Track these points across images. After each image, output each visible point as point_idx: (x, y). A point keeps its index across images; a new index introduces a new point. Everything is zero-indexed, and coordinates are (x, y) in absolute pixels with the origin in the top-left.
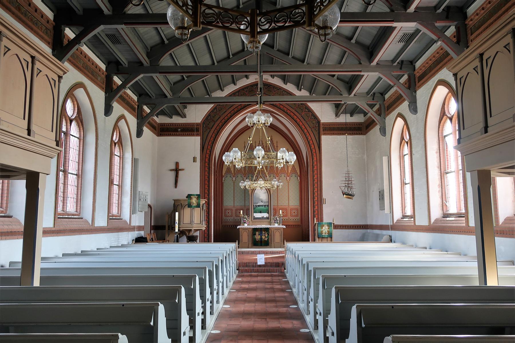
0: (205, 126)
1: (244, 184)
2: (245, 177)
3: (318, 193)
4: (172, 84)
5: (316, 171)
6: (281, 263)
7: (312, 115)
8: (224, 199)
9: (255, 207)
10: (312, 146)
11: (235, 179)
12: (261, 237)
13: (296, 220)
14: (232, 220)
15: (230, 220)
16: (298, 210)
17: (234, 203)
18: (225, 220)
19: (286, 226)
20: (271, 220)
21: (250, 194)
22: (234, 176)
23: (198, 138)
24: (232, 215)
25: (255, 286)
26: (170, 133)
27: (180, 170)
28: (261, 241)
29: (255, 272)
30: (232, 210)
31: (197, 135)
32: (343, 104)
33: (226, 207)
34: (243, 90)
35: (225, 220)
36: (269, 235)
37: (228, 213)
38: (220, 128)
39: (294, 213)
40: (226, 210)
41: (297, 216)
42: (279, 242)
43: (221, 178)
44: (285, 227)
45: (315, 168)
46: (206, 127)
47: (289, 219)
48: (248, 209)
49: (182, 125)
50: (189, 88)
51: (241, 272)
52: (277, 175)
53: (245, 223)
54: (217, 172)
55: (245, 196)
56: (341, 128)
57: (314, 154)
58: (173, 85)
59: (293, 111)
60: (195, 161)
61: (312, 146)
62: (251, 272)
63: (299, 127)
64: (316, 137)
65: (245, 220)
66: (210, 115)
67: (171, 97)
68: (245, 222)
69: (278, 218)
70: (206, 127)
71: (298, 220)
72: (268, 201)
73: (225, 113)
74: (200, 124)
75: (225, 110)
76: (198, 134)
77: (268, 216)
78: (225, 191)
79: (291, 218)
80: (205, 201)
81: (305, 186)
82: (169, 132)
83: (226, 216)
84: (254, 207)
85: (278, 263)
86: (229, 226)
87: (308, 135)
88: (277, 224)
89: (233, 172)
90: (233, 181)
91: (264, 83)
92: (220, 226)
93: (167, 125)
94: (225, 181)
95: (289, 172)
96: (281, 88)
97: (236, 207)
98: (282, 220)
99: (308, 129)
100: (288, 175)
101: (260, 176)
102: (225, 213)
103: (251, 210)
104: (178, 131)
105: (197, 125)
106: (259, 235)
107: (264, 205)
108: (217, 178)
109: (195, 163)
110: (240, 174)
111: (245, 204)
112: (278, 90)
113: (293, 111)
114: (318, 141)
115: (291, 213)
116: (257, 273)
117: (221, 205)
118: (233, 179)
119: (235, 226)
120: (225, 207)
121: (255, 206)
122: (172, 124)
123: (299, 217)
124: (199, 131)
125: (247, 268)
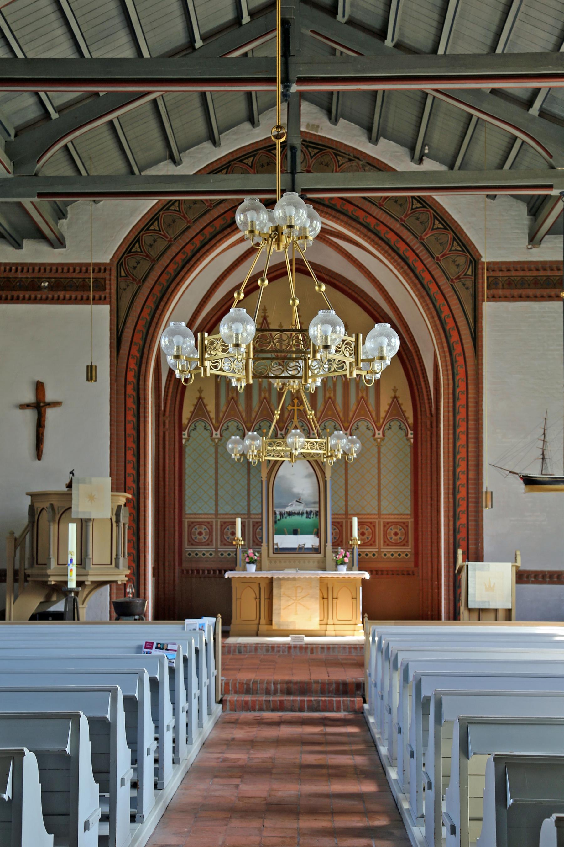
0: (123, 274)
1: (240, 447)
3: (470, 477)
4: (12, 133)
5: (463, 411)
6: (353, 683)
7: (454, 239)
8: (188, 492)
9: (278, 517)
10: (454, 334)
15: (197, 554)
18: (222, 555)
19: (371, 572)
20: (325, 556)
22: (216, 425)
23: (105, 309)
25: (270, 758)
26: (15, 294)
27: (49, 405)
29: (273, 710)
31: (99, 301)
32: (558, 199)
33: (192, 516)
34: (241, 161)
35: (190, 554)
38: (170, 280)
39: (396, 534)
40: (192, 525)
43: (177, 433)
45: (461, 402)
46: (126, 276)
48: (257, 523)
49: (54, 268)
50: (66, 146)
51: (231, 710)
54: (164, 415)
55: (249, 484)
56: (545, 278)
57: (460, 359)
58: (16, 135)
59: (397, 226)
60: (91, 379)
61: (454, 334)
62: (261, 710)
63: (414, 278)
64: (466, 307)
66: (138, 240)
67: (11, 176)
70: (126, 276)
71: (407, 555)
72: (318, 500)
73: (186, 233)
74: (108, 268)
75: (184, 226)
76: (103, 296)
77: (318, 544)
79: (385, 549)
80: (127, 499)
82: (14, 289)
83: (192, 543)
84: (276, 517)
85: (345, 684)
87: (441, 302)
89: (213, 415)
90: (213, 440)
91: (308, 139)
92: (177, 571)
93: (5, 268)
94: (190, 441)
95: (383, 414)
96: (358, 156)
97: (222, 516)
99: (442, 281)
100: (379, 425)
102: (190, 533)
103: (267, 525)
104: (40, 288)
105: (100, 271)
107: (307, 512)
108: (164, 433)
109: (92, 383)
110: (235, 421)
112: (350, 160)
113: (397, 226)
114: (471, 320)
115: (385, 534)
116: (280, 714)
117: (177, 510)
118: (214, 436)
119: (220, 571)
121: (278, 513)
122: (22, 267)
123: (409, 549)
124: (104, 289)
125: (249, 698)
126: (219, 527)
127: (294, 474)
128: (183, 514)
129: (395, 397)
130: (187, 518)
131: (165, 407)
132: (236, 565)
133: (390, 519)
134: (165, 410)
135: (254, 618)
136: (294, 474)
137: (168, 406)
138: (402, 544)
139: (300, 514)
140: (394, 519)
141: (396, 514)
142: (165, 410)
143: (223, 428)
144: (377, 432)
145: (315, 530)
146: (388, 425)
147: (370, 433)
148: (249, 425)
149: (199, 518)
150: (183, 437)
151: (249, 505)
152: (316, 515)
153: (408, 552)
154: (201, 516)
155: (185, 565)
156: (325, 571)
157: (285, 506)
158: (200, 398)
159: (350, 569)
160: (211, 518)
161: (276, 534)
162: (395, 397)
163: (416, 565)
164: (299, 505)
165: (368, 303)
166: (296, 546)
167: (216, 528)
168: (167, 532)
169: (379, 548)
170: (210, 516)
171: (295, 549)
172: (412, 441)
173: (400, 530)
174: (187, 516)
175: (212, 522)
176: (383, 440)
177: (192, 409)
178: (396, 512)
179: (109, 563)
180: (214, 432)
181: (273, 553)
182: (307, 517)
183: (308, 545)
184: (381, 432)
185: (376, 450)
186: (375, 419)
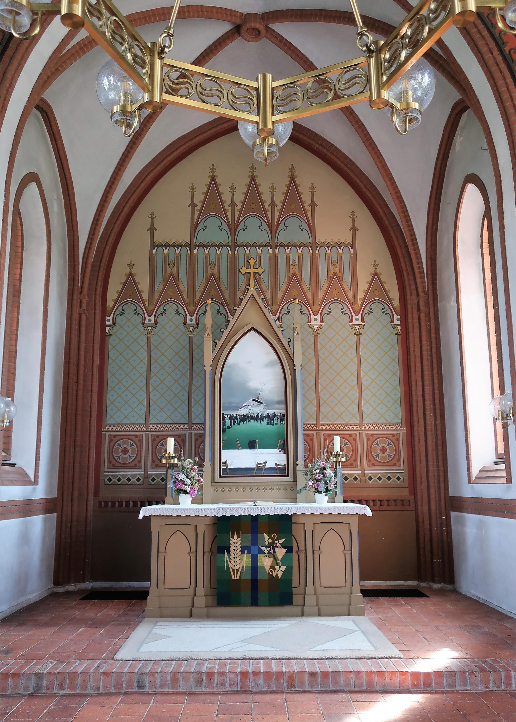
8: (111, 396)
9: (228, 423)
11: (153, 322)
12: (255, 560)
13: (389, 478)
14: (138, 480)
15: (119, 480)
16: (397, 439)
17: (148, 413)
18: (110, 480)
20: (295, 480)
21: (208, 369)
22: (150, 308)
24: (140, 462)
28: (255, 582)
33: (115, 428)
35: (153, 480)
36: (295, 549)
37: (125, 451)
39: (383, 450)
41: (394, 465)
42: (343, 583)
44: (368, 512)
47: (363, 475)
52: (315, 308)
53: (181, 491)
55: (191, 384)
65: (182, 477)
68: (183, 487)
69: (329, 472)
72: (284, 398)
77: (284, 463)
78: (112, 367)
79: (370, 471)
81: (424, 348)
83: (114, 464)
84: (224, 424)
86: (128, 503)
88: (326, 498)
89: (146, 296)
90: (145, 327)
92: (91, 503)
94: (117, 327)
95: (361, 295)
97: (154, 427)
98: (346, 479)
100: (356, 308)
102: (111, 451)
106: (243, 552)
107: (268, 416)
115: (369, 450)
119: (135, 504)
120: (111, 427)
123: (402, 469)
127: (250, 362)
129: (376, 274)
130: (108, 431)
131: (83, 282)
132: (166, 495)
133: (375, 429)
134: (82, 287)
136: (250, 362)
137: (87, 281)
138: (392, 463)
139: (259, 418)
140: (380, 429)
141: (382, 424)
142: (82, 287)
143: (159, 312)
144: (354, 317)
145: (280, 442)
146: (368, 307)
147: (347, 319)
148: (192, 308)
149: (124, 430)
150: (107, 323)
151: (190, 412)
152: (282, 420)
153: (400, 474)
154: (127, 428)
155: (103, 494)
156: (296, 502)
157: (238, 408)
159: (332, 500)
160: (140, 431)
162: (376, 274)
164: (257, 406)
165: (339, 159)
166: (254, 466)
167: (147, 445)
168: (78, 449)
170: (138, 428)
171: (252, 469)
173: (389, 444)
174: (107, 428)
176: (362, 326)
177: (120, 288)
180: (147, 318)
181: (220, 476)
182: (268, 424)
183: (271, 465)
184: (359, 317)
185: (354, 340)
186: (352, 301)
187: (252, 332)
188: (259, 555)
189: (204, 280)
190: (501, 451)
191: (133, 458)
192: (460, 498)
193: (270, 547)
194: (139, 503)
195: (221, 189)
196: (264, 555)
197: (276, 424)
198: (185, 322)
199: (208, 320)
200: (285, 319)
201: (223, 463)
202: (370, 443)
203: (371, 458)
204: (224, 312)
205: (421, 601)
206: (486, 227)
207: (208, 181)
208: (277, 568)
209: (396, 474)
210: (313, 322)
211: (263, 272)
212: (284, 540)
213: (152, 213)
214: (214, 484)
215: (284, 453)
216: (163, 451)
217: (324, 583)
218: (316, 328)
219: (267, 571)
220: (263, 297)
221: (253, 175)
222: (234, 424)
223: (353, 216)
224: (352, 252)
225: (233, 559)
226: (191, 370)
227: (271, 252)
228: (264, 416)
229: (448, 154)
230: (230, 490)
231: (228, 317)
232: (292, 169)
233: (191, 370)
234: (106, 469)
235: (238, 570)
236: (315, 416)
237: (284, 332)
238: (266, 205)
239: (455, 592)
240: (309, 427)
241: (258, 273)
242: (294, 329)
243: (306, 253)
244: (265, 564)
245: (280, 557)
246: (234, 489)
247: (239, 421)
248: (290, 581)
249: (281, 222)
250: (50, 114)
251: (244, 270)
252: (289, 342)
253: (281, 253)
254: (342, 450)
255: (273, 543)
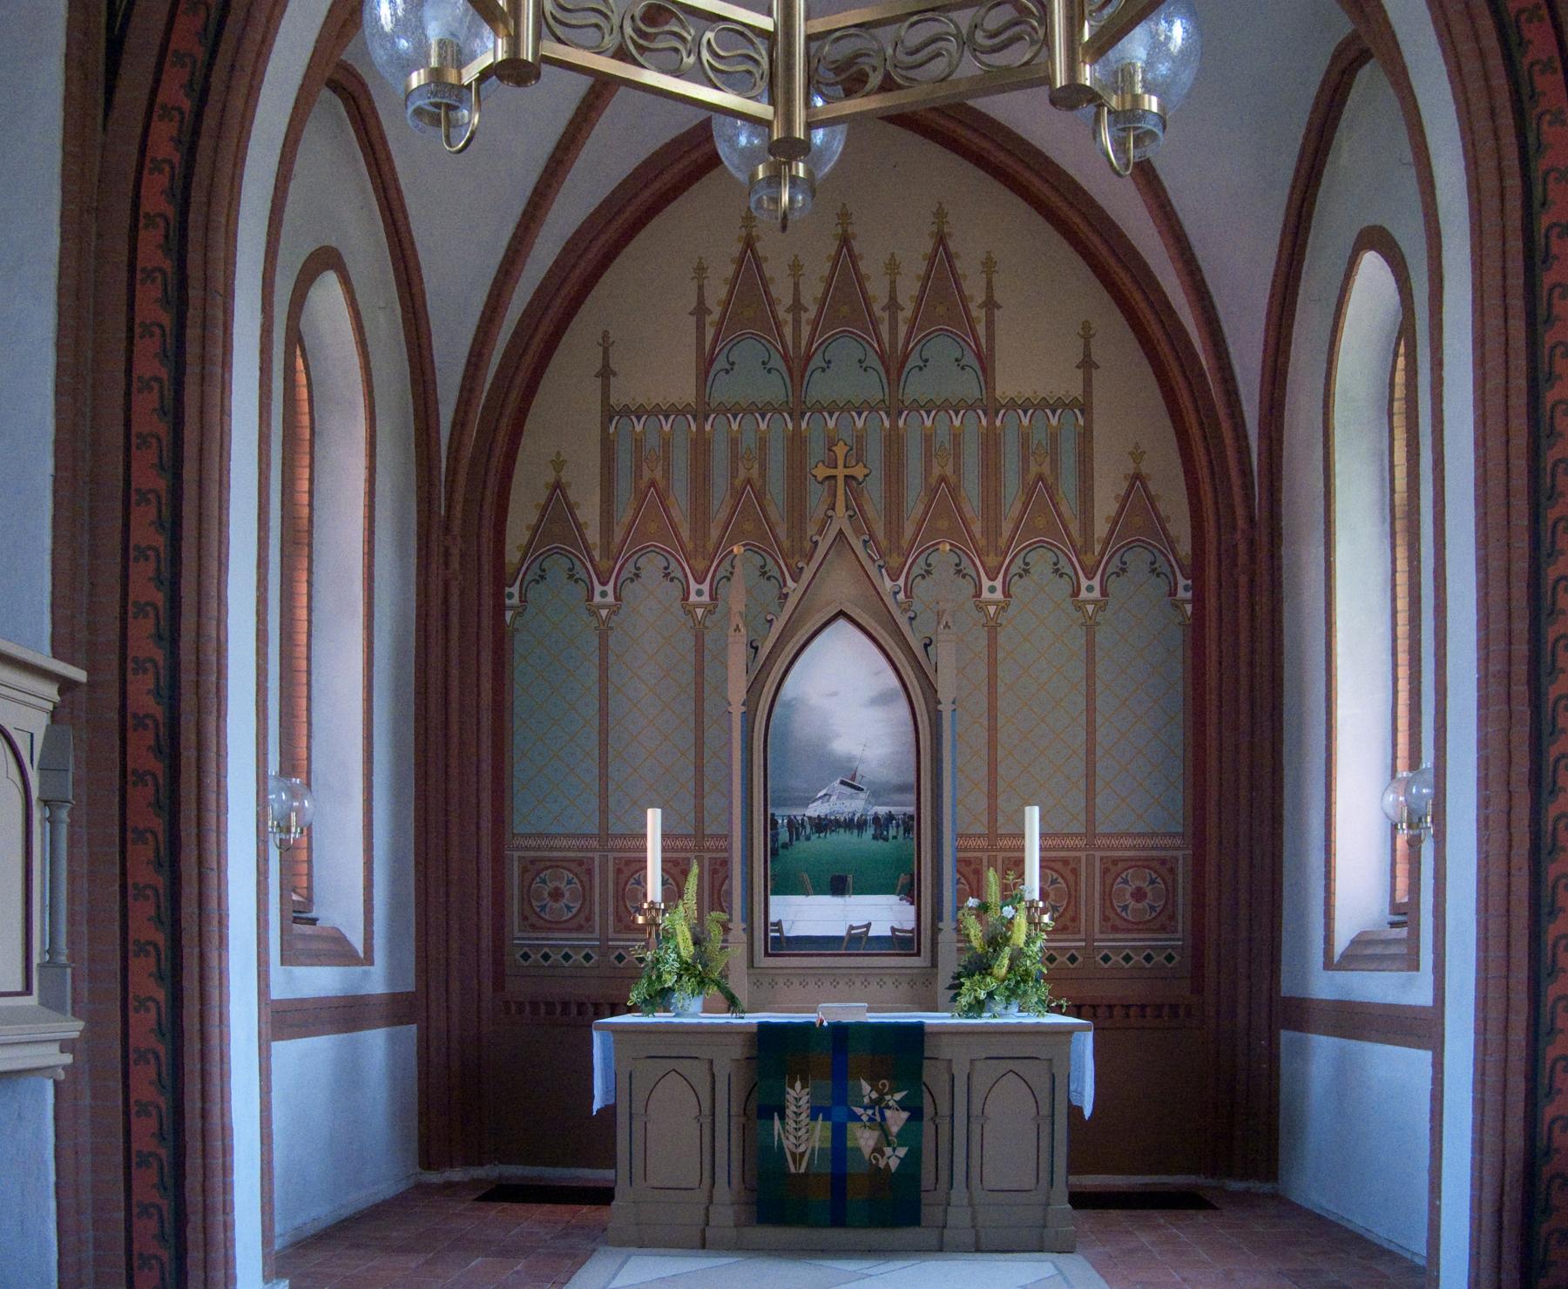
2: (700, 581)
8: (521, 770)
9: (784, 836)
11: (610, 599)
12: (839, 1133)
14: (588, 957)
22: (604, 565)
30: (590, 872)
33: (532, 843)
36: (928, 1110)
40: (532, 868)
42: (1029, 1182)
43: (487, 590)
52: (992, 561)
54: (447, 529)
72: (912, 778)
77: (910, 924)
83: (532, 921)
84: (775, 837)
95: (1101, 529)
100: (1089, 560)
101: (832, 533)
106: (814, 1117)
107: (876, 819)
111: (700, 820)
115: (1107, 896)
123: (1177, 940)
126: (611, 875)
127: (834, 694)
128: (508, 836)
130: (518, 848)
131: (449, 507)
135: (693, 1181)
136: (834, 694)
139: (853, 825)
144: (1084, 583)
148: (700, 565)
150: (508, 602)
151: (699, 809)
152: (908, 830)
154: (556, 843)
158: (558, 486)
161: (775, 893)
162: (1137, 476)
163: (1198, 989)
164: (851, 797)
166: (843, 933)
169: (1089, 939)
172: (1189, 608)
174: (516, 842)
175: (592, 859)
176: (1101, 606)
178: (1139, 828)
179: (19, 988)
180: (598, 588)
181: (767, 954)
182: (875, 837)
183: (880, 929)
186: (1079, 542)
187: (842, 623)
188: (851, 1126)
189: (728, 497)
190: (1402, 897)
191: (574, 911)
192: (1304, 1000)
193: (872, 1107)
194: (591, 1009)
195: (768, 270)
196: (858, 1124)
197: (895, 837)
198: (686, 597)
199: (736, 598)
200: (921, 587)
201: (773, 924)
202: (1108, 881)
203: (1109, 912)
204: (775, 572)
205: (1201, 1217)
206: (1401, 362)
207: (736, 249)
208: (888, 1151)
209: (1164, 948)
210: (986, 595)
211: (866, 476)
212: (904, 1093)
213: (605, 335)
214: (751, 971)
215: (912, 904)
216: (641, 896)
217: (992, 1180)
218: (992, 609)
219: (867, 1157)
220: (867, 538)
221: (845, 231)
222: (798, 839)
223: (1087, 335)
224: (1081, 422)
225: (791, 1130)
226: (699, 713)
227: (887, 424)
228: (866, 821)
229: (1320, 173)
230: (788, 983)
231: (785, 585)
232: (940, 215)
233: (699, 713)
234: (517, 934)
235: (802, 1154)
236: (985, 819)
237: (914, 623)
238: (877, 309)
239: (1278, 1198)
240: (972, 843)
241: (853, 478)
242: (939, 615)
243: (971, 425)
244: (862, 1143)
245: (895, 1129)
246: (796, 981)
247: (808, 831)
248: (916, 1178)
249: (913, 349)
250: (364, 103)
251: (822, 472)
252: (926, 646)
253: (914, 426)
254: (1044, 895)
255: (881, 1099)
